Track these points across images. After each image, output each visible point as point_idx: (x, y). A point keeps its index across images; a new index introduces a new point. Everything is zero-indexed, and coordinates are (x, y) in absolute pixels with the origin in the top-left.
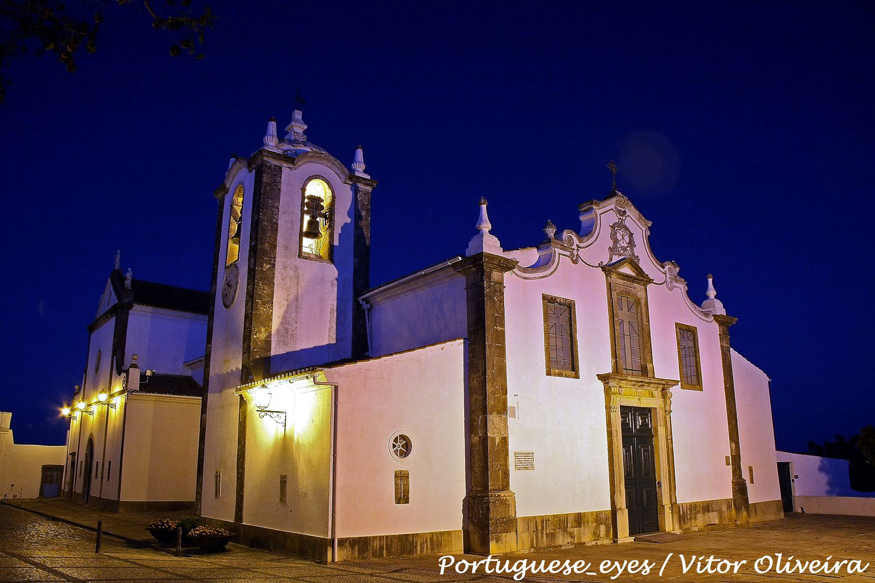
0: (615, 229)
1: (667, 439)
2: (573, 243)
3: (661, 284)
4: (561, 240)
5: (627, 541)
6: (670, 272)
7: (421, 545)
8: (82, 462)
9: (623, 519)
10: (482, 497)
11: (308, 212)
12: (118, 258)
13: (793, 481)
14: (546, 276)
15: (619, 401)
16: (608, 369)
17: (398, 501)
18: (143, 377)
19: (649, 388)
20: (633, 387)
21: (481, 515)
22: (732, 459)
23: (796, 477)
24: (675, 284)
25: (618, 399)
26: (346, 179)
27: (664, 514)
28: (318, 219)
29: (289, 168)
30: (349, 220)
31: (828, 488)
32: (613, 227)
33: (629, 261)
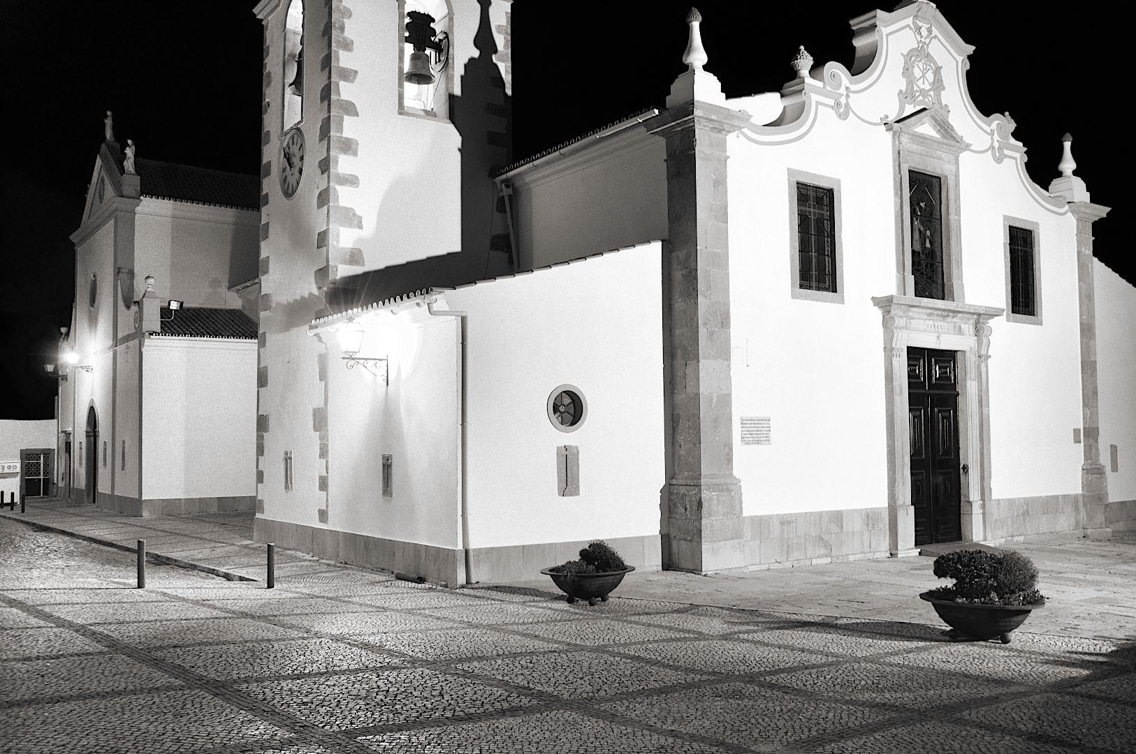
2: (841, 84)
11: (407, 40)
12: (109, 122)
17: (563, 493)
18: (165, 312)
19: (955, 320)
20: (929, 318)
28: (428, 52)
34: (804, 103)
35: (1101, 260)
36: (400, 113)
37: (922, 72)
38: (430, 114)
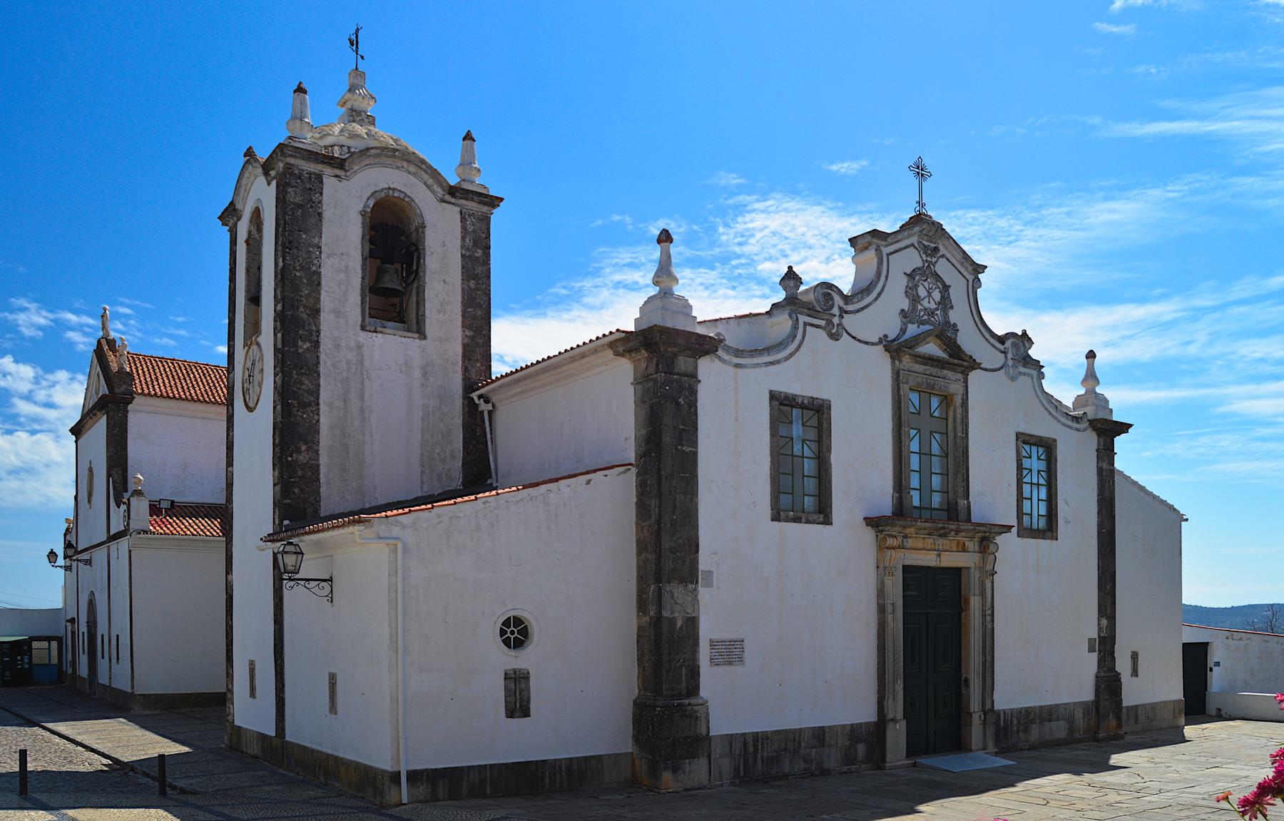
0: (914, 279)
1: (984, 616)
3: (995, 370)
6: (1014, 350)
7: (550, 777)
8: (83, 633)
9: (897, 736)
13: (1211, 670)
14: (778, 362)
17: (511, 714)
20: (928, 536)
22: (1099, 642)
23: (1218, 664)
24: (1022, 369)
27: (971, 725)
29: (336, 176)
32: (910, 276)
33: (936, 333)
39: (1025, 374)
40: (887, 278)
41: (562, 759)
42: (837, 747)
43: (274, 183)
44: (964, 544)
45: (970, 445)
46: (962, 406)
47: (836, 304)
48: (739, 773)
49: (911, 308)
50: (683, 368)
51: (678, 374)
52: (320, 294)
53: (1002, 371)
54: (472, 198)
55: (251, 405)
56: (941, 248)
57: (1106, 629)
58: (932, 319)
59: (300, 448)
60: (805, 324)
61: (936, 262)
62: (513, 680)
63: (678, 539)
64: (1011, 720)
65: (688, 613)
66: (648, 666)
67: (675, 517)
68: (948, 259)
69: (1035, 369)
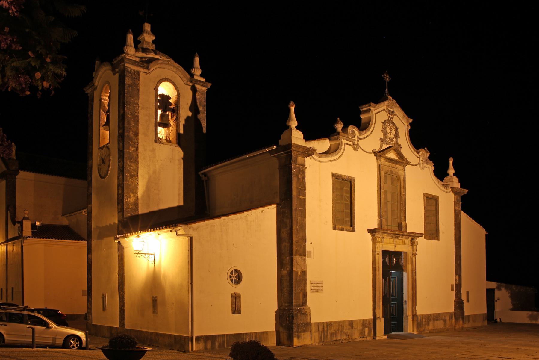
0: (385, 125)
1: (413, 273)
3: (415, 165)
4: (347, 133)
5: (382, 338)
6: (423, 156)
9: (380, 325)
10: (289, 310)
11: (159, 108)
13: (496, 301)
15: (381, 247)
16: (375, 226)
17: (234, 313)
18: (34, 226)
19: (403, 239)
20: (391, 238)
21: (288, 321)
24: (425, 165)
25: (381, 245)
26: (187, 82)
27: (408, 321)
29: (145, 72)
30: (190, 114)
31: (147, 232)
32: (384, 123)
34: (339, 144)
35: (465, 212)
36: (156, 141)
37: (390, 130)
38: (168, 141)
39: (427, 167)
40: (375, 124)
41: (253, 333)
42: (358, 329)
43: (117, 75)
44: (405, 242)
45: (406, 198)
46: (403, 181)
47: (356, 135)
48: (321, 339)
49: (384, 138)
50: (300, 162)
51: (298, 165)
52: (138, 126)
53: (418, 165)
54: (199, 83)
55: (103, 175)
56: (395, 111)
57: (458, 280)
58: (392, 142)
59: (130, 196)
60: (345, 144)
61: (393, 117)
62: (234, 298)
63: (298, 237)
64: (423, 320)
65: (302, 269)
66: (286, 293)
67: (297, 227)
68: (397, 116)
69: (430, 165)
